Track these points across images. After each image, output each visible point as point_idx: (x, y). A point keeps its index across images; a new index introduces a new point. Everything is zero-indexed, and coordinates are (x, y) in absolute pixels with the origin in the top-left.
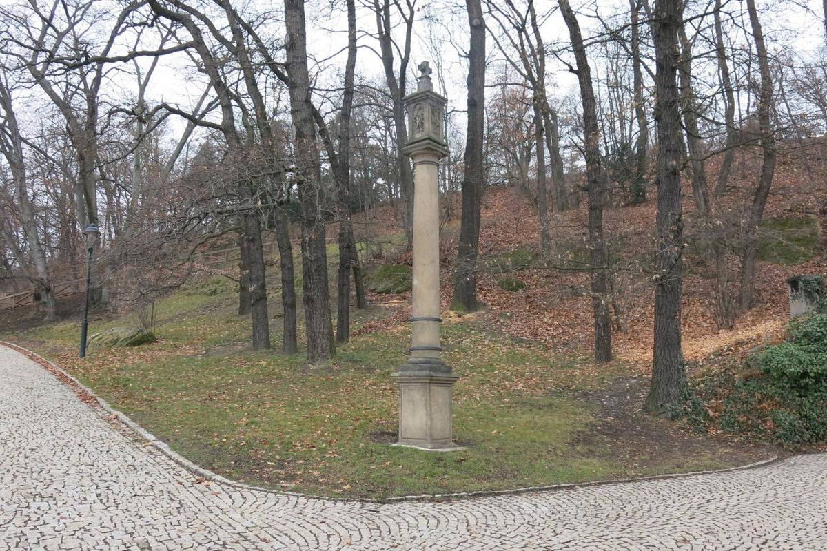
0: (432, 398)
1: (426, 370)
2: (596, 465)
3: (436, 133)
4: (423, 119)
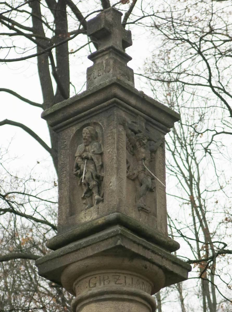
2: (159, 153)
3: (142, 209)
4: (102, 166)
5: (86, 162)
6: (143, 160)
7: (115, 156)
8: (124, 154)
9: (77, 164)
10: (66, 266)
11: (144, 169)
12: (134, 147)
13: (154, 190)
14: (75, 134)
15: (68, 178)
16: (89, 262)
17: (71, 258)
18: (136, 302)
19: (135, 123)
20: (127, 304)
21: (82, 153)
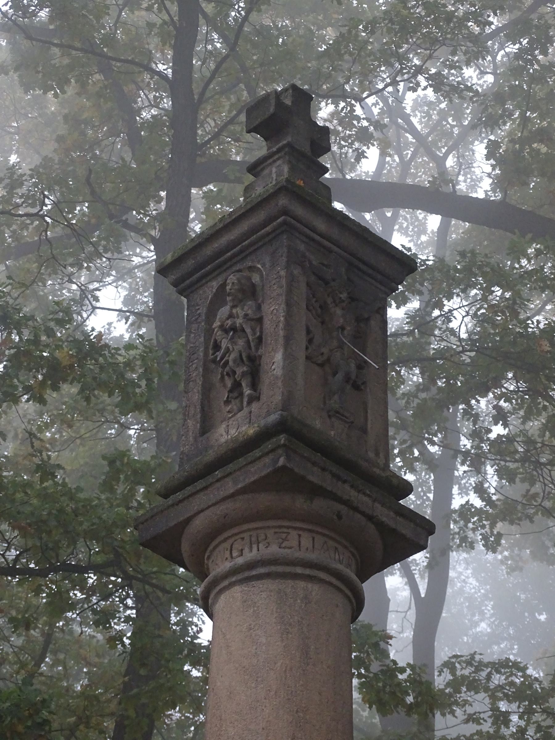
4: (260, 340)
5: (231, 334)
6: (340, 330)
7: (283, 316)
9: (216, 341)
10: (188, 521)
11: (341, 346)
12: (324, 307)
13: (362, 387)
14: (215, 294)
15: (201, 370)
17: (197, 503)
18: (321, 581)
19: (326, 266)
20: (302, 584)
21: (225, 321)
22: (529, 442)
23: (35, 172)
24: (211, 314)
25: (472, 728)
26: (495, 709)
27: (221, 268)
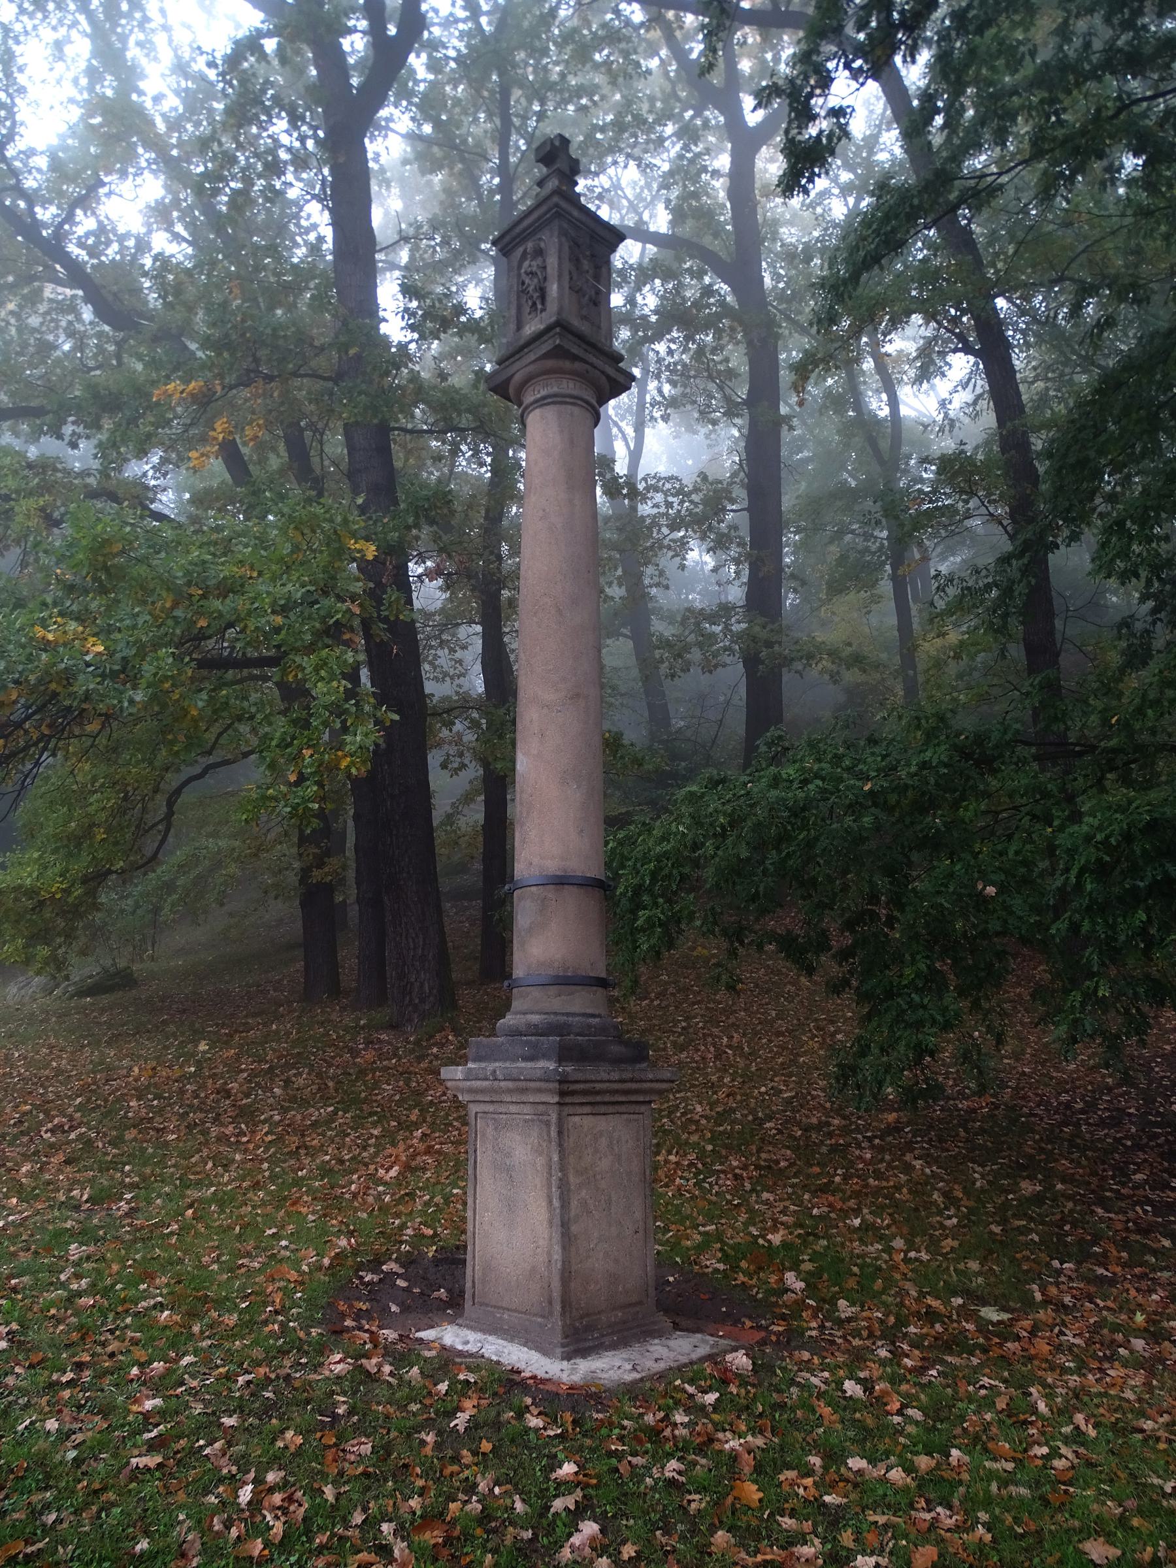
0: (572, 1159)
1: (545, 1056)
2: (604, 270)
3: (584, 318)
4: (545, 279)
8: (567, 265)
12: (578, 260)
16: (531, 368)
22: (684, 365)
23: (430, 221)
24: (520, 267)
25: (655, 511)
26: (666, 501)
27: (525, 240)
